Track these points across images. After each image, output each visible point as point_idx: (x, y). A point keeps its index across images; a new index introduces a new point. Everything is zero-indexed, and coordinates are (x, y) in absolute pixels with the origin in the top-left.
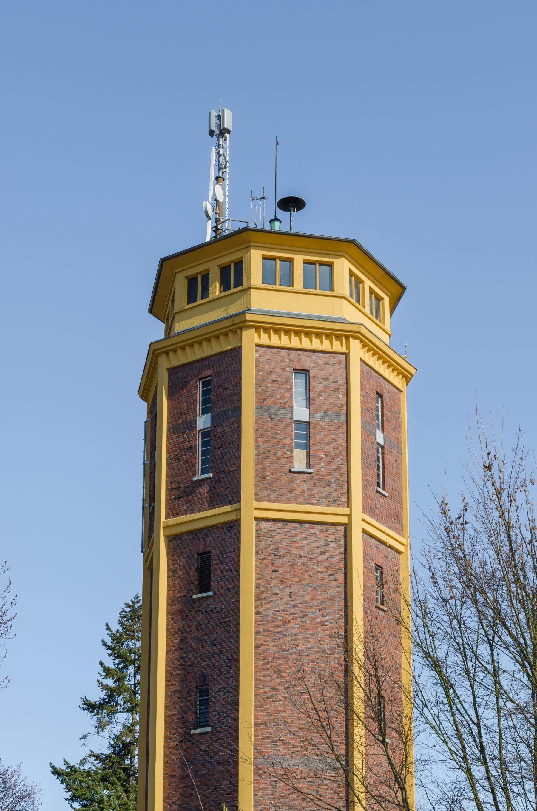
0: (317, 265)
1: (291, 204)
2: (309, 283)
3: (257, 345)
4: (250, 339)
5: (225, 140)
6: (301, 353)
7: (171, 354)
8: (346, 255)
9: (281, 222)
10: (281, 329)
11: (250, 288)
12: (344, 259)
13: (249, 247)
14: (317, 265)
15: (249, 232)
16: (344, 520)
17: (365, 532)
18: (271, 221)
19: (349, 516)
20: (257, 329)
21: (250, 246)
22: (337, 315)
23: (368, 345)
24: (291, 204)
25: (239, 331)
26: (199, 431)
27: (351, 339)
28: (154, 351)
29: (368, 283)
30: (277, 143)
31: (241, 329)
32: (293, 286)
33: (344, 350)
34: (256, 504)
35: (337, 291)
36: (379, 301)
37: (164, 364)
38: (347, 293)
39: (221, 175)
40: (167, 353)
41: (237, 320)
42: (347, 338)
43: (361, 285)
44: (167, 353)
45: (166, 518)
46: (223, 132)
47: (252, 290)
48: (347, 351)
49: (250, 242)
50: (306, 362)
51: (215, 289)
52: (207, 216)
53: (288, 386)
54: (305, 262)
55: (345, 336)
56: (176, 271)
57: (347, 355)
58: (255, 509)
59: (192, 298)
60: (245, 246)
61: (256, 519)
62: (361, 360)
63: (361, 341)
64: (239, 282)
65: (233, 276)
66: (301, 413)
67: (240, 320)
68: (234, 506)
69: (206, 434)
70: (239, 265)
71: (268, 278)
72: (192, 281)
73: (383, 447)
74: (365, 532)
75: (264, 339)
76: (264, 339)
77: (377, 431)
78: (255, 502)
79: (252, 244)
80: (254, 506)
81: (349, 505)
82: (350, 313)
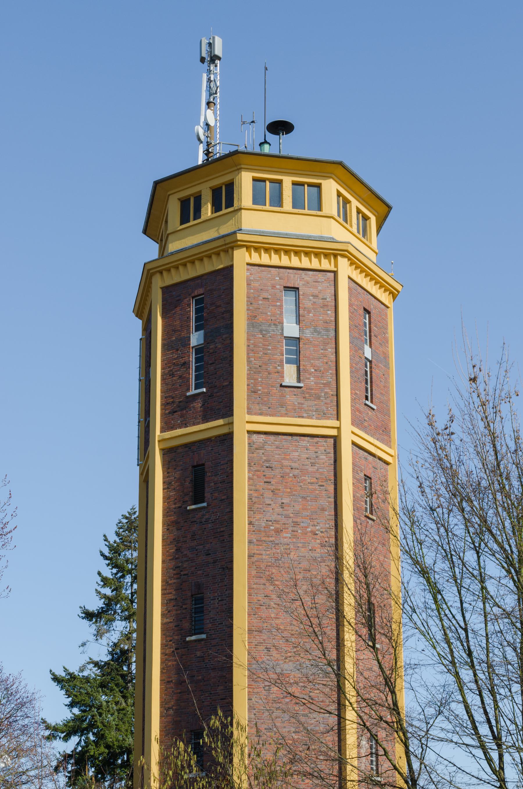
0: (306, 186)
1: (281, 127)
2: (297, 203)
3: (248, 264)
4: (241, 258)
5: (216, 66)
6: (291, 271)
7: (165, 273)
8: (333, 176)
9: (270, 145)
10: (251, 246)
11: (240, 209)
12: (331, 180)
13: (239, 170)
14: (306, 186)
15: (240, 155)
16: (334, 432)
17: (354, 444)
18: (261, 144)
19: (339, 429)
20: (248, 248)
21: (241, 168)
22: (326, 235)
23: (355, 263)
24: (281, 127)
25: (230, 251)
26: (193, 347)
27: (339, 257)
28: (149, 270)
29: (355, 203)
30: (266, 69)
31: (232, 248)
32: (282, 207)
33: (333, 268)
34: (248, 418)
35: (326, 210)
36: (366, 220)
37: (158, 283)
38: (335, 213)
39: (212, 100)
40: (161, 273)
41: (228, 240)
42: (335, 256)
43: (348, 205)
44: (161, 273)
45: (161, 432)
46: (214, 59)
47: (243, 211)
48: (335, 269)
49: (240, 164)
50: (295, 279)
51: (207, 210)
52: (199, 139)
53: (278, 304)
54: (294, 184)
55: (333, 255)
56: (169, 193)
57: (335, 273)
58: (247, 422)
59: (184, 219)
60: (236, 168)
61: (249, 432)
62: (349, 278)
63: (349, 259)
64: (230, 203)
65: (225, 197)
66: (291, 329)
67: (234, 240)
68: (226, 420)
69: (199, 350)
70: (230, 187)
71: (258, 199)
72: (184, 203)
73: (371, 362)
74: (354, 444)
75: (255, 258)
76: (255, 258)
77: (365, 346)
78: (247, 416)
79: (243, 166)
80: (247, 420)
81: (338, 418)
82: (339, 233)
